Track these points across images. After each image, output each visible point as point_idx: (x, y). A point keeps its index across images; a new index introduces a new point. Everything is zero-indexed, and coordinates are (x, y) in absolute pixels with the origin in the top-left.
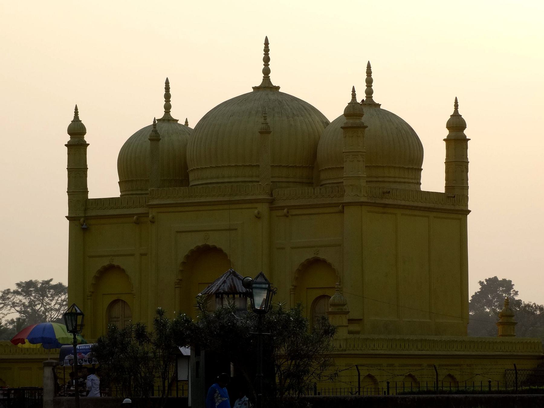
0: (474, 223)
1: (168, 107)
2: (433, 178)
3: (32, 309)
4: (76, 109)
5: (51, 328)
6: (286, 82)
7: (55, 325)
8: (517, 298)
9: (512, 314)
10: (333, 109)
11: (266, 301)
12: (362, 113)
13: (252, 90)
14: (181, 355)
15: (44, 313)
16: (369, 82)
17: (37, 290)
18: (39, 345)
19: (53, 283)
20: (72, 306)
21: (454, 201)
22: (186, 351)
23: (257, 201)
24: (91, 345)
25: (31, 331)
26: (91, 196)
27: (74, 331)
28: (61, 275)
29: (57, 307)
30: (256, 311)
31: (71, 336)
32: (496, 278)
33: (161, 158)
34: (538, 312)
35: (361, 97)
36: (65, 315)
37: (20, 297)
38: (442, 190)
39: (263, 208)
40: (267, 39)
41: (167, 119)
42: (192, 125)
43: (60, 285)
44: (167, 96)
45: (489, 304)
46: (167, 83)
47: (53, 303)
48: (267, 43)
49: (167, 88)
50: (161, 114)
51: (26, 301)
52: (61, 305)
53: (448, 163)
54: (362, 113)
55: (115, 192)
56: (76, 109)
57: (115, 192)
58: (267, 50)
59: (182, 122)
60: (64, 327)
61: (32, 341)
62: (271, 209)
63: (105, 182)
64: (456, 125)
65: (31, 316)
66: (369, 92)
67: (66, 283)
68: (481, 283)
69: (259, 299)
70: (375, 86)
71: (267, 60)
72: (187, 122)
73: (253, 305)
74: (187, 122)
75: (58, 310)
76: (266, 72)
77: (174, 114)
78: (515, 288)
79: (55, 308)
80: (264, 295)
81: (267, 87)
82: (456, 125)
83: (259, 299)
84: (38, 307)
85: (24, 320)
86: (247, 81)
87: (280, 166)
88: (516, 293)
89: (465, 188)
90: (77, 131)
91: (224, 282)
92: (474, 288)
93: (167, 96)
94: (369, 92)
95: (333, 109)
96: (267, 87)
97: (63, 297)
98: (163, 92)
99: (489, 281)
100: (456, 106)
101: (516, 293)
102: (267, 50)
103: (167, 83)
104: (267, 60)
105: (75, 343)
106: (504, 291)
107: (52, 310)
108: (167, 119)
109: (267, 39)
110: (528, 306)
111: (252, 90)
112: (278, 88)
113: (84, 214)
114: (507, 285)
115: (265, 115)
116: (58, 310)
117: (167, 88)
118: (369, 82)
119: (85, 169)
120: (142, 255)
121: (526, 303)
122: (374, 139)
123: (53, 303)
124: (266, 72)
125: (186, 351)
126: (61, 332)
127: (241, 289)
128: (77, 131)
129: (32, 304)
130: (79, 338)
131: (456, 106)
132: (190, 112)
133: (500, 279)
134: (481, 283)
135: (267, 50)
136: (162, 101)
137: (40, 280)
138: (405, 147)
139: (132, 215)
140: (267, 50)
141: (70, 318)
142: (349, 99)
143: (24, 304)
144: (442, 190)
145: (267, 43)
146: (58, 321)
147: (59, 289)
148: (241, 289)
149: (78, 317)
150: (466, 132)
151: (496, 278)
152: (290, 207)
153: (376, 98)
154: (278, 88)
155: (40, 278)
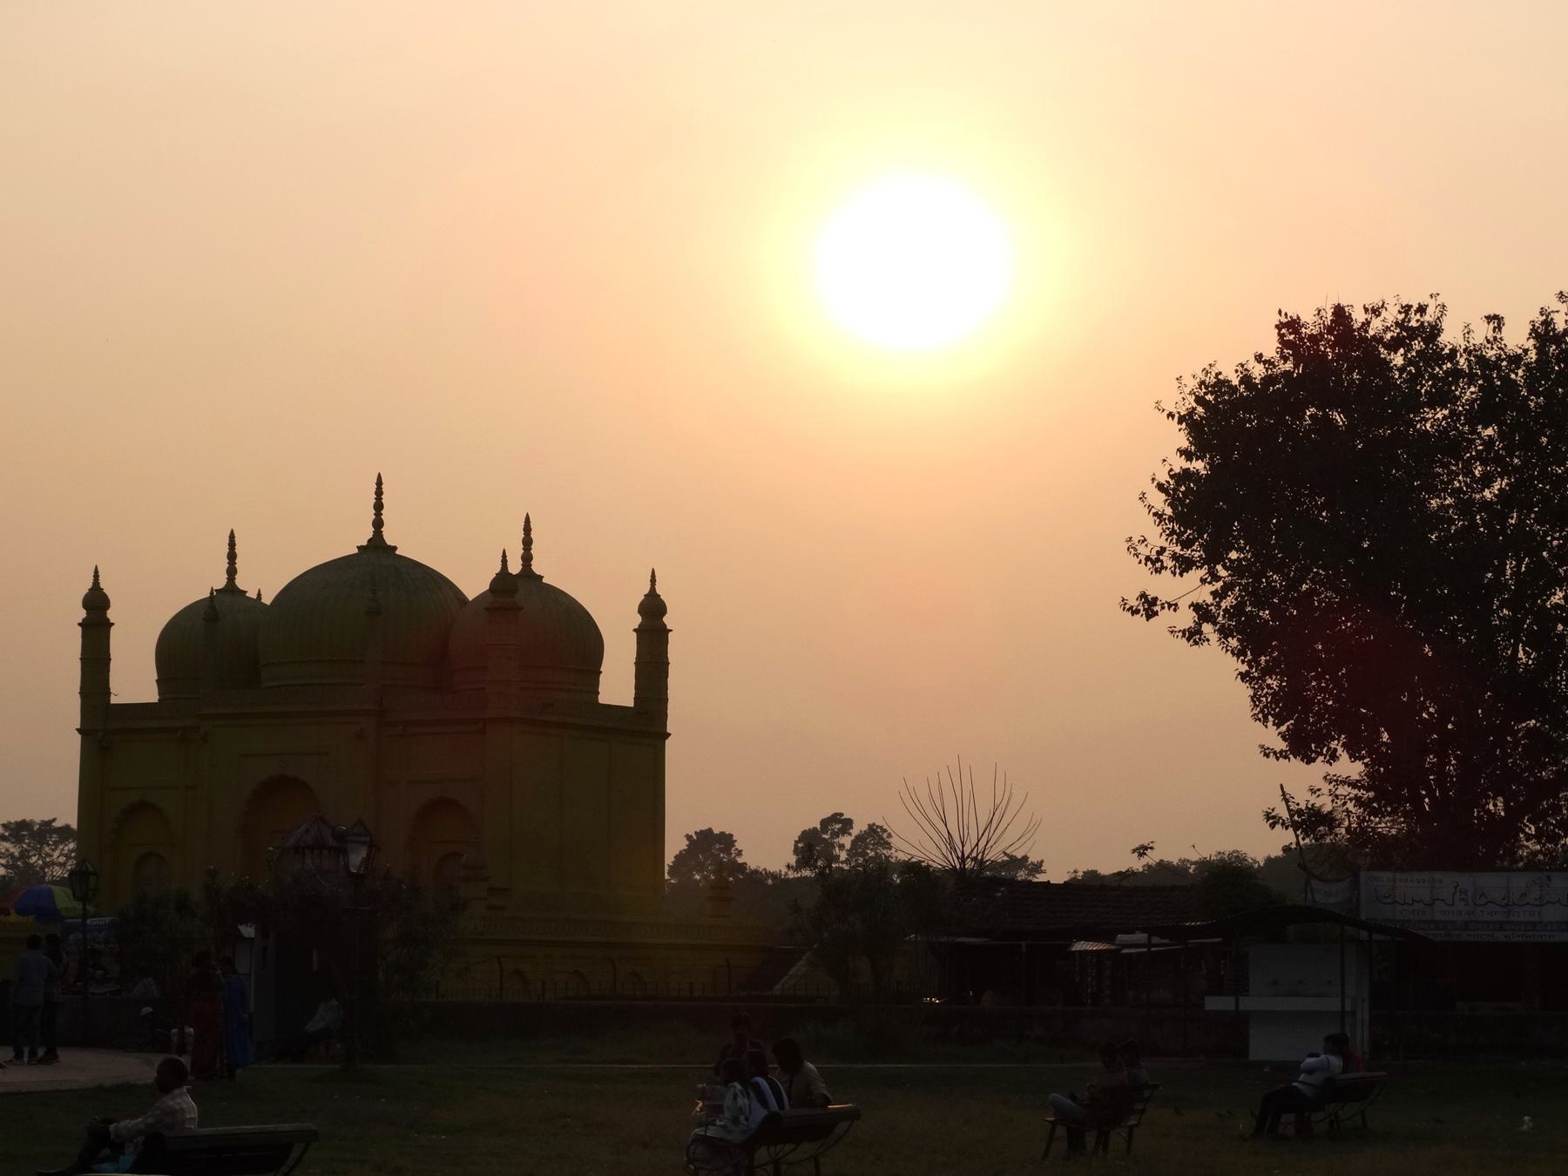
0: (673, 750)
1: (232, 572)
2: (617, 684)
3: (25, 863)
4: (96, 572)
5: (50, 895)
6: (406, 541)
7: (56, 889)
8: (740, 860)
9: (1339, 485)
10: (473, 582)
11: (366, 861)
12: (519, 590)
14: (241, 936)
15: (42, 868)
16: (527, 542)
17: (33, 835)
18: (31, 918)
19: (57, 824)
20: (81, 862)
21: (649, 713)
22: (248, 931)
24: (108, 920)
25: (22, 894)
26: (114, 700)
27: (83, 898)
28: (66, 813)
29: (62, 859)
30: (352, 875)
31: (79, 905)
32: (710, 830)
33: (218, 641)
34: (770, 882)
35: (515, 567)
36: (72, 873)
37: (7, 845)
38: (631, 704)
40: (379, 477)
41: (231, 589)
42: (267, 600)
43: (67, 827)
44: (232, 556)
45: (700, 868)
46: (232, 537)
47: (56, 854)
48: (379, 483)
49: (232, 544)
50: (221, 582)
51: (16, 851)
52: (68, 857)
53: (640, 664)
54: (519, 590)
55: (151, 695)
56: (96, 572)
57: (151, 695)
58: (379, 493)
59: (252, 594)
60: (69, 891)
61: (20, 912)
63: (135, 679)
64: (653, 608)
65: (22, 870)
66: (527, 558)
67: (74, 826)
68: (689, 837)
69: (356, 858)
70: (535, 550)
71: (379, 506)
72: (259, 595)
73: (347, 867)
74: (259, 595)
75: (62, 865)
76: (378, 524)
77: (240, 582)
78: (738, 845)
79: (59, 860)
80: (363, 854)
81: (377, 546)
82: (653, 608)
83: (356, 858)
84: (34, 859)
85: (12, 879)
86: (349, 539)
88: (740, 853)
89: (664, 701)
90: (96, 602)
91: (307, 831)
92: (674, 844)
93: (232, 556)
94: (527, 558)
95: (473, 582)
96: (377, 546)
97: (72, 846)
99: (700, 834)
100: (653, 580)
101: (740, 853)
102: (379, 492)
103: (232, 537)
104: (379, 506)
105: (85, 916)
106: (722, 850)
107: (53, 864)
108: (231, 589)
109: (379, 477)
110: (756, 872)
112: (395, 548)
113: (102, 721)
114: (727, 840)
115: (375, 587)
116: (62, 865)
117: (232, 544)
118: (527, 542)
119: (107, 660)
121: (753, 867)
122: (533, 623)
123: (56, 854)
124: (378, 524)
125: (248, 931)
126: (64, 899)
127: (331, 842)
128: (96, 602)
129: (24, 855)
130: (90, 908)
131: (653, 580)
132: (265, 580)
133: (716, 831)
134: (689, 837)
135: (379, 492)
136: (225, 564)
137: (38, 819)
138: (577, 636)
140: (379, 493)
141: (79, 878)
142: (498, 568)
143: (12, 855)
144: (631, 704)
145: (379, 483)
146: (61, 882)
147: (65, 833)
148: (331, 842)
150: (665, 619)
151: (710, 830)
153: (537, 567)
154: (395, 548)
155: (37, 815)
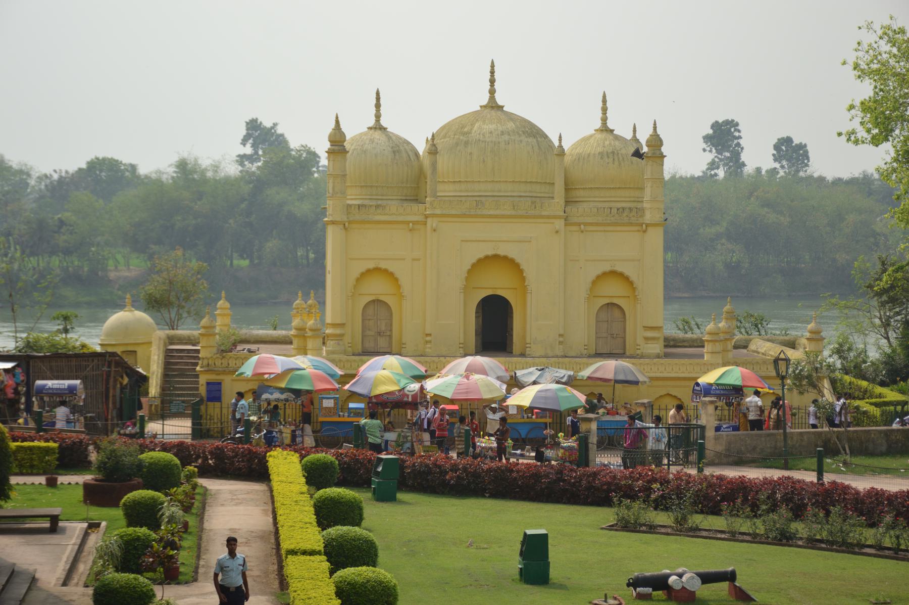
13: (479, 108)
23: (555, 217)
39: (559, 224)
49: (604, 101)
62: (566, 225)
71: (492, 82)
76: (492, 92)
87: (526, 182)
98: (374, 102)
102: (492, 72)
103: (378, 94)
111: (479, 108)
112: (503, 107)
117: (604, 101)
120: (414, 260)
136: (373, 110)
139: (408, 223)
145: (493, 66)
149: (815, 474)
152: (586, 224)
154: (503, 107)
